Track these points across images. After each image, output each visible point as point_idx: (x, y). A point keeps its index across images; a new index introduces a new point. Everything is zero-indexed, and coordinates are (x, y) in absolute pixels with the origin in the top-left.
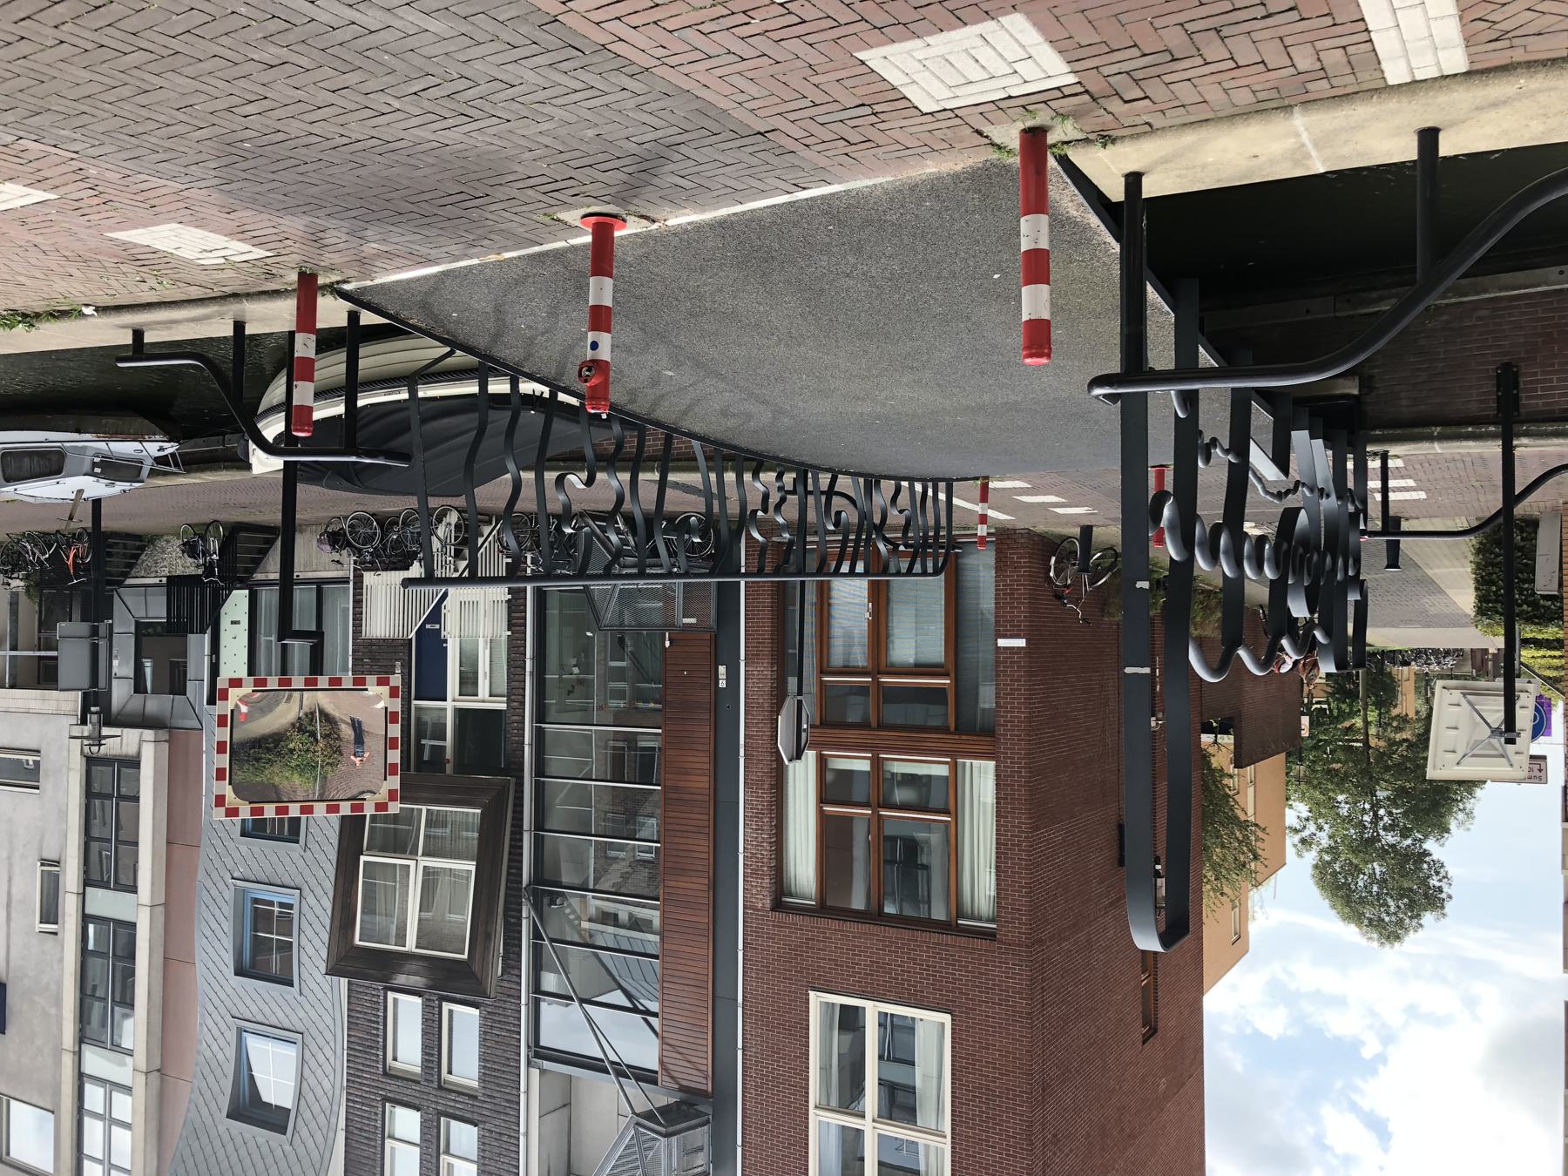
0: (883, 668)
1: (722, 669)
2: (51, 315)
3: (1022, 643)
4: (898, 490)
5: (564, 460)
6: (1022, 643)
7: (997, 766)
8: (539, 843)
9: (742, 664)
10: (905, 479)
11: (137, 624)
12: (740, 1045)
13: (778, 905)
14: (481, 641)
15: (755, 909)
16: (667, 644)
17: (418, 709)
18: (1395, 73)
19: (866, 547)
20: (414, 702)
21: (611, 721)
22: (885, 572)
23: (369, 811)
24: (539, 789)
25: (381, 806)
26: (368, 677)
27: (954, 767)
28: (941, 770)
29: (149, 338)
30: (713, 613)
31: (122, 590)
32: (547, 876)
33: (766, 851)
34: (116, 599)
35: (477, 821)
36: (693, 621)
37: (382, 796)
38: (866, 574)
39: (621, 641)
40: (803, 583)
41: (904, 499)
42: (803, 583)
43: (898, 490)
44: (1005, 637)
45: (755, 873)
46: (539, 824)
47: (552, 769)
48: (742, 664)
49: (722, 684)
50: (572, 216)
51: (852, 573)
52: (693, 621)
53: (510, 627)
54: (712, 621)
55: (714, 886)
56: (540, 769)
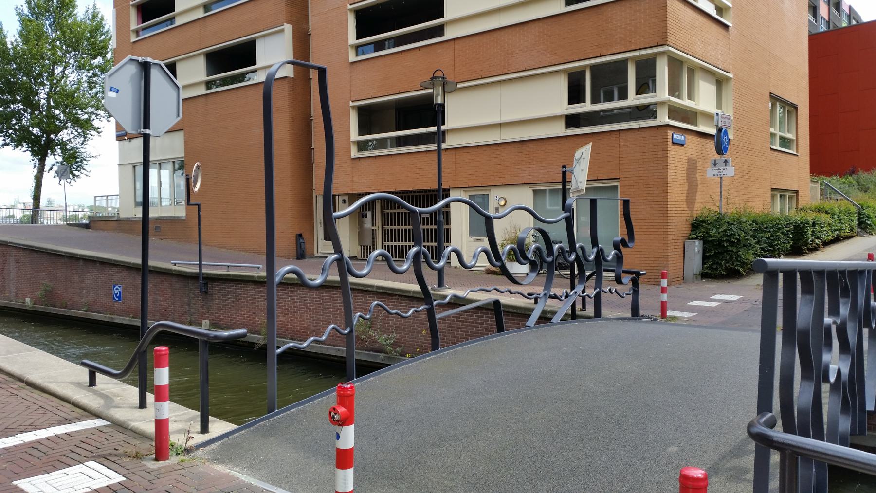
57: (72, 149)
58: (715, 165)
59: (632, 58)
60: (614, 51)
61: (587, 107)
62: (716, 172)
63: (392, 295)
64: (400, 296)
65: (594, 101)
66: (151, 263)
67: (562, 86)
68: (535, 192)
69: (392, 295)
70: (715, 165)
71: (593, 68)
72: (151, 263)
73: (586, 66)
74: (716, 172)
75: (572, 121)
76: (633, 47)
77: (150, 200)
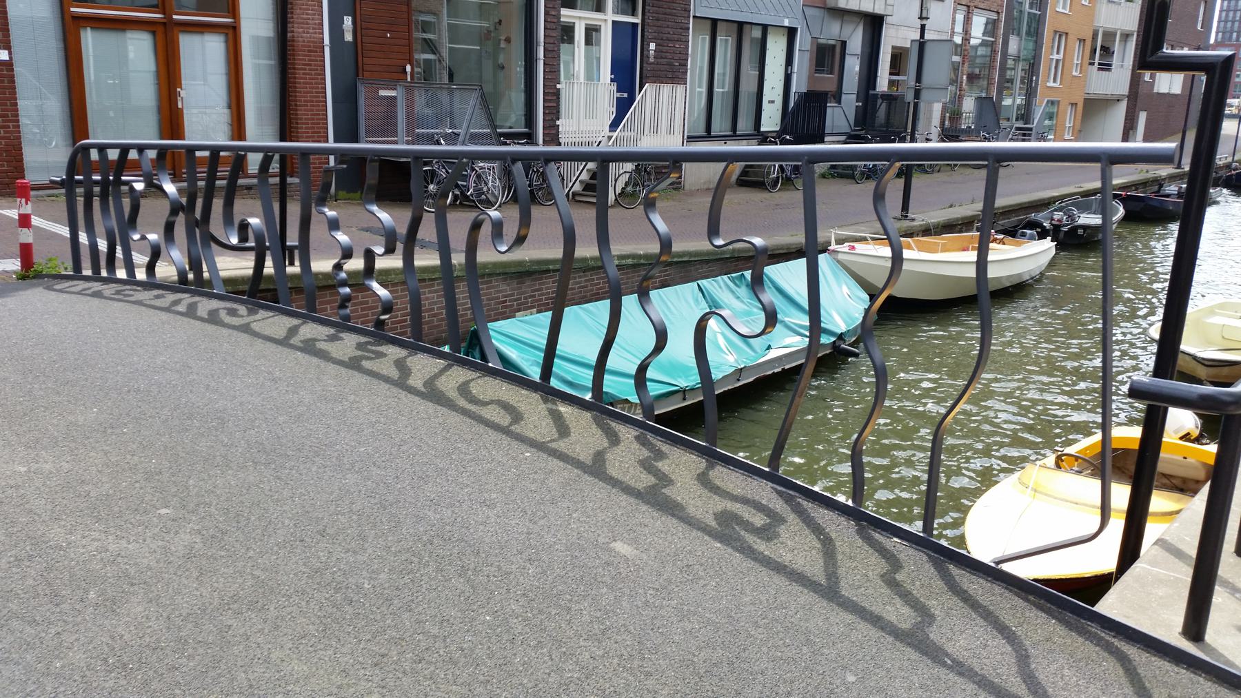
0: (160, 29)
1: (349, 37)
2: (769, 563)
4: (151, 268)
5: (548, 271)
9: (327, 41)
10: (140, 283)
11: (839, 102)
12: (1201, 18)
14: (582, 79)
16: (408, 68)
17: (633, 14)
18: (881, 286)
19: (211, 180)
20: (637, 20)
22: (162, 152)
31: (848, 131)
34: (852, 123)
36: (383, 93)
38: (191, 150)
39: (1107, 51)
41: (140, 259)
43: (151, 268)
48: (327, 41)
49: (348, 21)
52: (383, 93)
54: (362, 91)
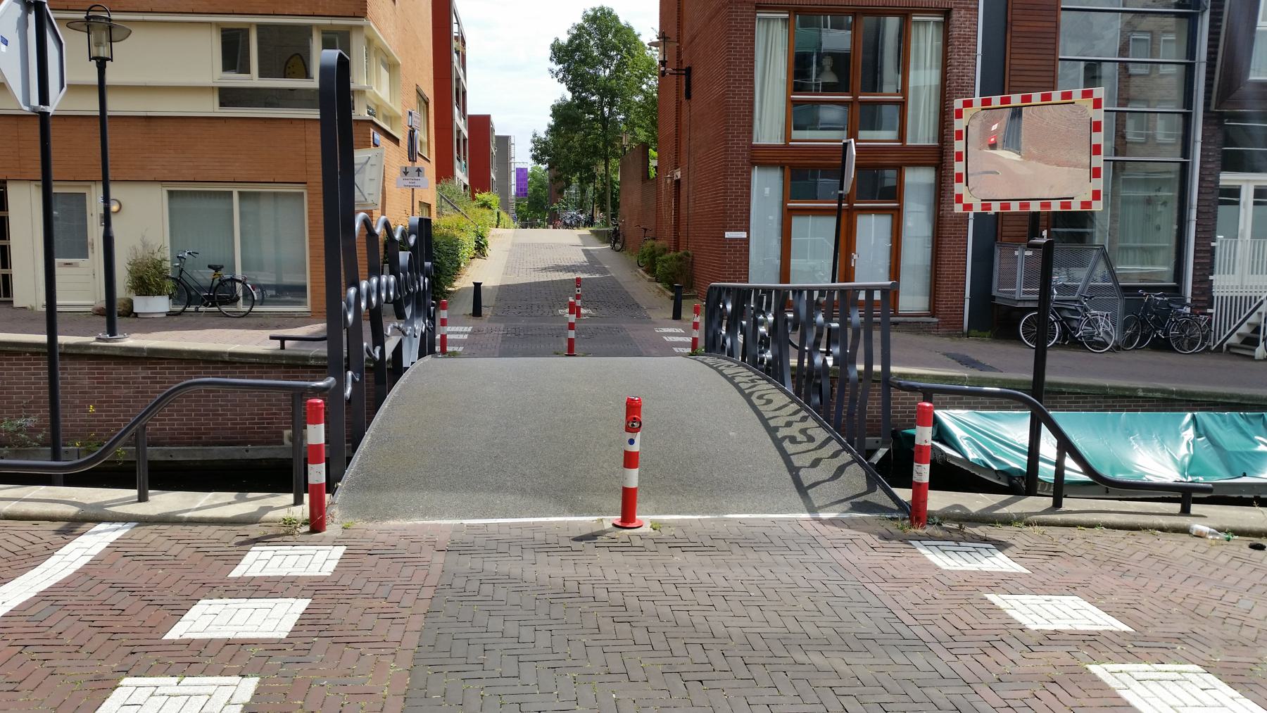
3: (728, 235)
6: (728, 235)
7: (751, 139)
8: (1191, 51)
13: (947, 13)
15: (967, 9)
21: (1128, 166)
23: (977, 100)
24: (1188, 100)
25: (968, 104)
26: (1059, 209)
27: (788, 137)
28: (796, 134)
29: (1177, 507)
30: (997, 260)
32: (1185, 22)
33: (955, 58)
35: (1251, 72)
37: (967, 113)
38: (856, 290)
40: (833, 281)
42: (833, 281)
44: (741, 239)
45: (967, 39)
46: (1190, 69)
47: (1178, 120)
50: (646, 529)
51: (870, 291)
53: (1212, 251)
55: (1006, 25)
56: (1187, 118)
57: (559, 62)
58: (406, 173)
59: (318, 26)
60: (294, 11)
61: (252, 80)
62: (407, 183)
63: (17, 353)
64: (32, 354)
65: (262, 74)
66: (62, 339)
67: (211, 47)
68: (171, 193)
69: (17, 353)
70: (406, 173)
71: (260, 27)
72: (1049, 378)
73: (250, 24)
74: (407, 183)
75: (228, 97)
76: (320, 12)
77: (358, 196)
